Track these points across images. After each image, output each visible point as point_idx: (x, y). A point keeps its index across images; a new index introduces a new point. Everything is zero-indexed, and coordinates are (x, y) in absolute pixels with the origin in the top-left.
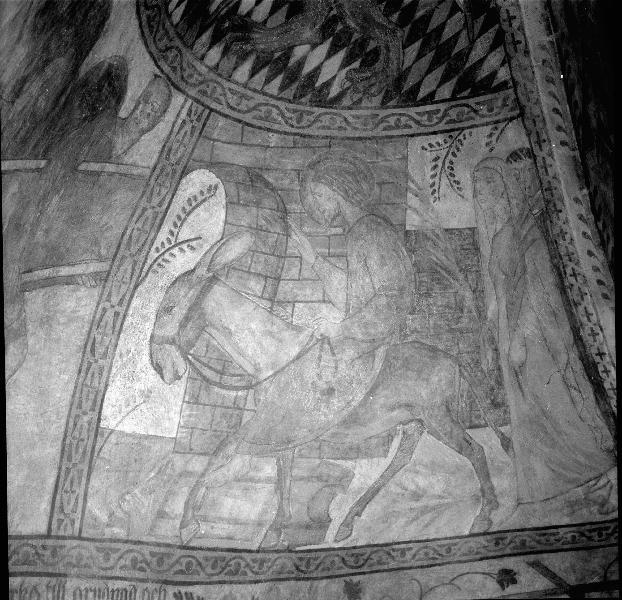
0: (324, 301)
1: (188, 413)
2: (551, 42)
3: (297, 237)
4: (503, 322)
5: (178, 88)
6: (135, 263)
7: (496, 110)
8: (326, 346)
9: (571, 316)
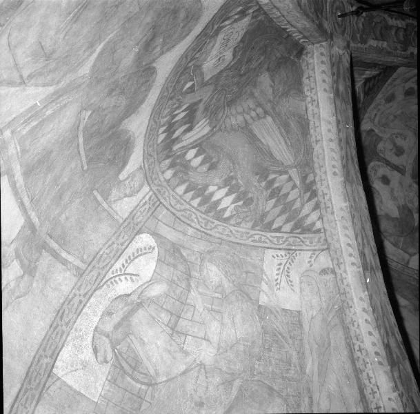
0: (205, 339)
1: (108, 388)
2: (346, 206)
3: (193, 294)
4: (316, 378)
5: (148, 184)
6: (99, 274)
7: (314, 244)
8: (202, 370)
9: (359, 380)
